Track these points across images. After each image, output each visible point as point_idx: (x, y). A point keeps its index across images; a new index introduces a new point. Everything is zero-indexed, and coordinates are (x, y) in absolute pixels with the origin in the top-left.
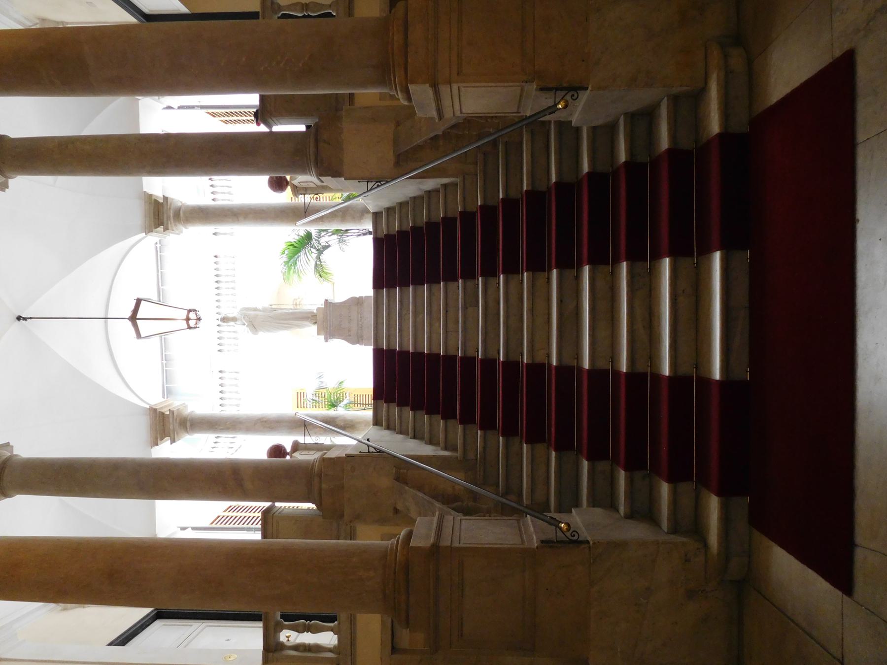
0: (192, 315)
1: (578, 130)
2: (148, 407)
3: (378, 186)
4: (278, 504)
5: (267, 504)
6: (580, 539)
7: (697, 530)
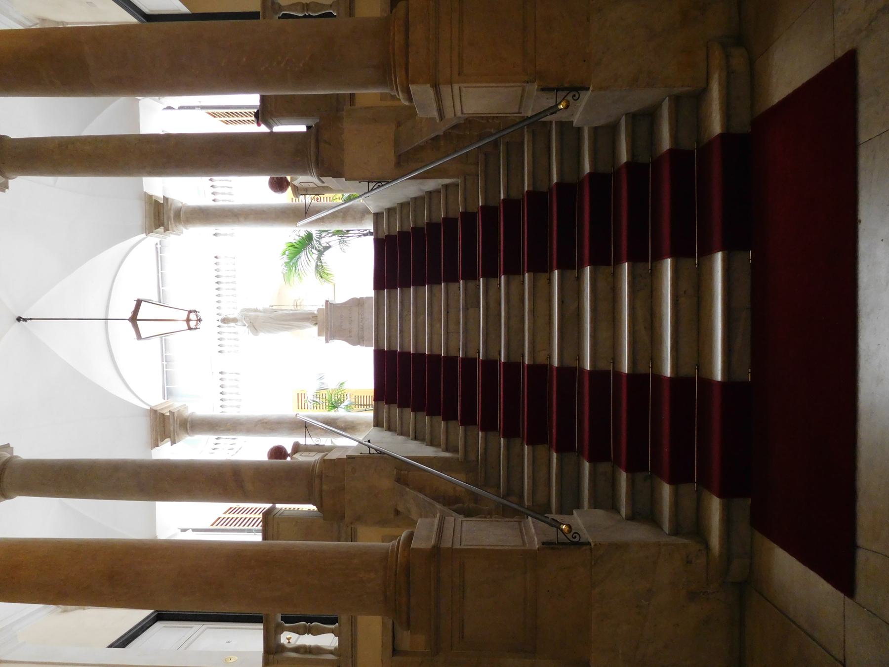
0: (193, 316)
1: (579, 130)
2: (148, 408)
3: (379, 187)
4: (278, 506)
5: (268, 506)
6: (581, 541)
7: (699, 532)
